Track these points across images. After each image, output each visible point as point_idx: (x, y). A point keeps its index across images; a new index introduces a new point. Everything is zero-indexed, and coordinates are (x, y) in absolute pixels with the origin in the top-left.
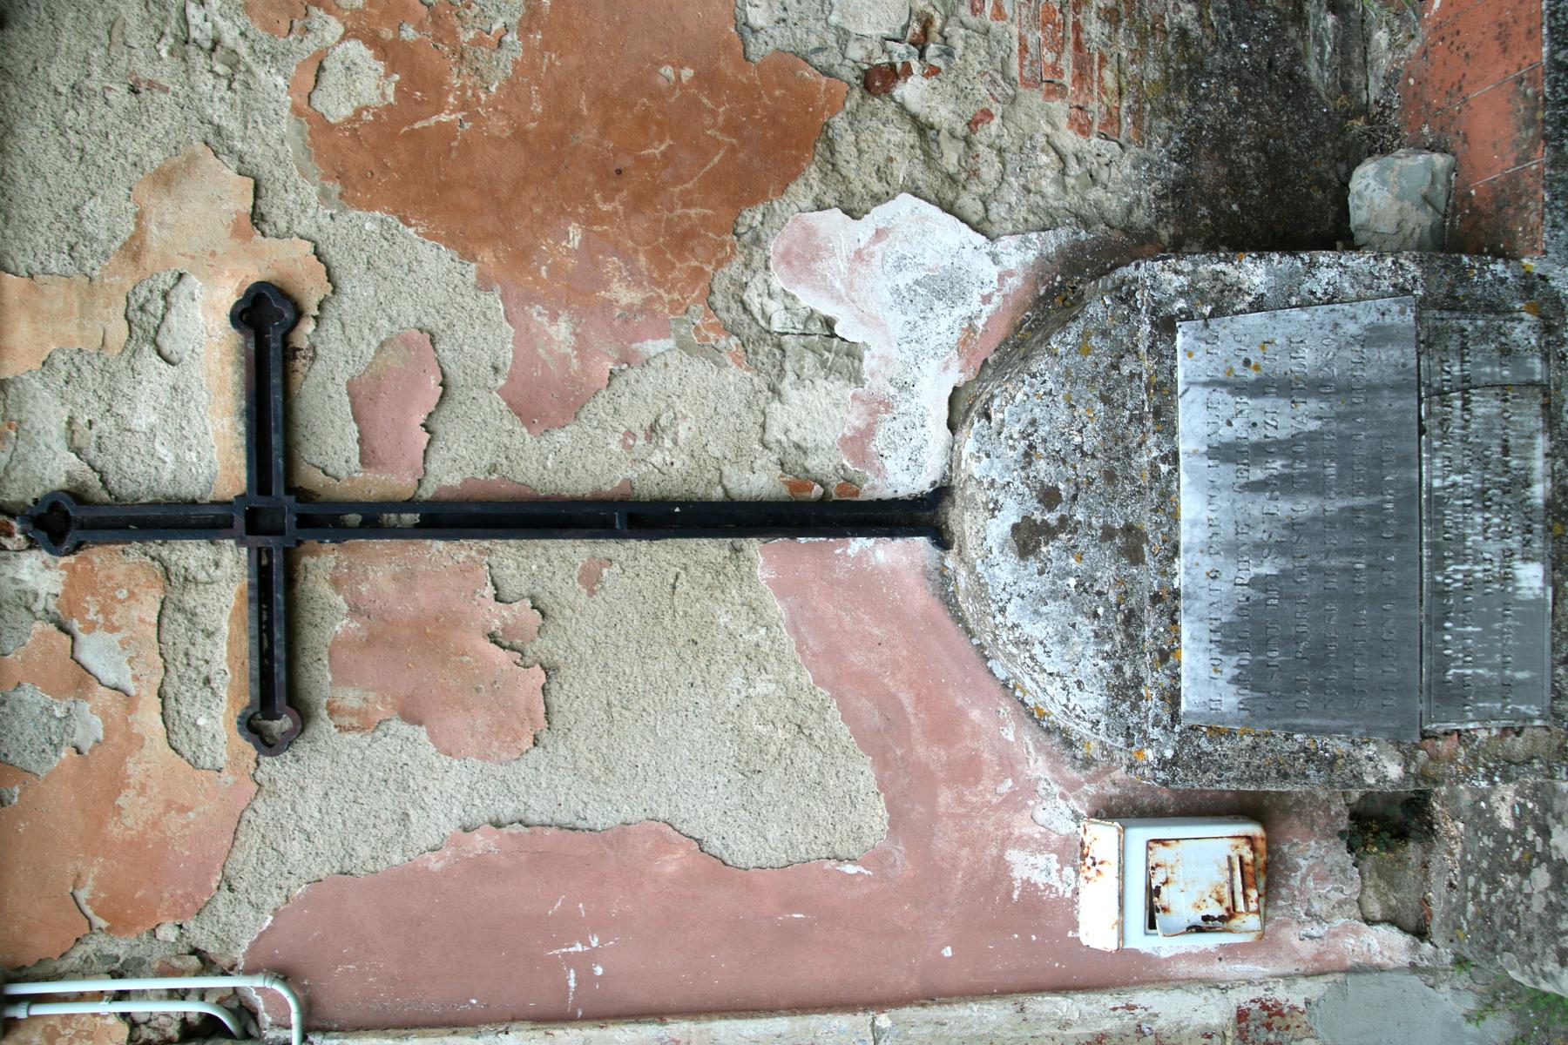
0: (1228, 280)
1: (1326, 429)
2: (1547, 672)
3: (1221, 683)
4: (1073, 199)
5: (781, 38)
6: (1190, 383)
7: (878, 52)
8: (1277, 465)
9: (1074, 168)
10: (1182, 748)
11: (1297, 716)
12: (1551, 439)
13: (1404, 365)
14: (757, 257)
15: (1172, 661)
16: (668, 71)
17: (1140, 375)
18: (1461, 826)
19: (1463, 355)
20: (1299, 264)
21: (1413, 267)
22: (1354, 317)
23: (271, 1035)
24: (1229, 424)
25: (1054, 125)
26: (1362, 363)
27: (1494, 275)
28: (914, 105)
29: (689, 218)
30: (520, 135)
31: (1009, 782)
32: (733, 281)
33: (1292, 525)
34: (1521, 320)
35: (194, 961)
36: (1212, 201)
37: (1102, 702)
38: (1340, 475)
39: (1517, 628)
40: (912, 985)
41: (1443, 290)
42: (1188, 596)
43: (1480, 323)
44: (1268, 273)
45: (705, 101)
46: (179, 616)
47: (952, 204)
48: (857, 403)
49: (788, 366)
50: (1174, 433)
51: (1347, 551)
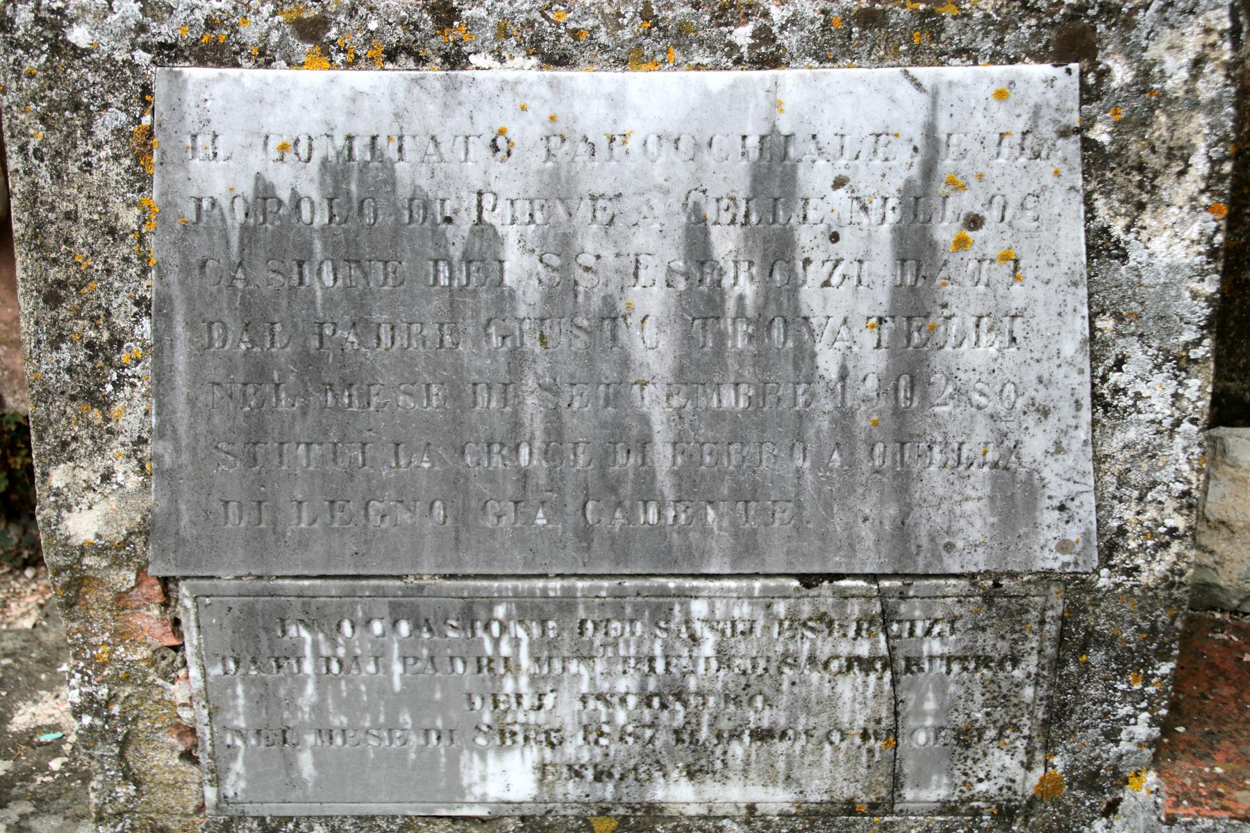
0: (1165, 182)
1: (820, 388)
2: (316, 809)
3: (257, 161)
6: (935, 95)
8: (743, 286)
10: (96, 67)
11: (191, 325)
12: (784, 815)
13: (949, 547)
15: (303, 48)
18: (27, 623)
19: (963, 659)
20: (1189, 335)
21: (1160, 568)
22: (1059, 449)
24: (839, 183)
26: (959, 464)
27: (1126, 720)
33: (611, 316)
34: (1028, 767)
38: (718, 416)
39: (402, 754)
41: (1103, 626)
42: (451, 87)
43: (1028, 692)
44: (1173, 269)
50: (822, 58)
51: (555, 430)
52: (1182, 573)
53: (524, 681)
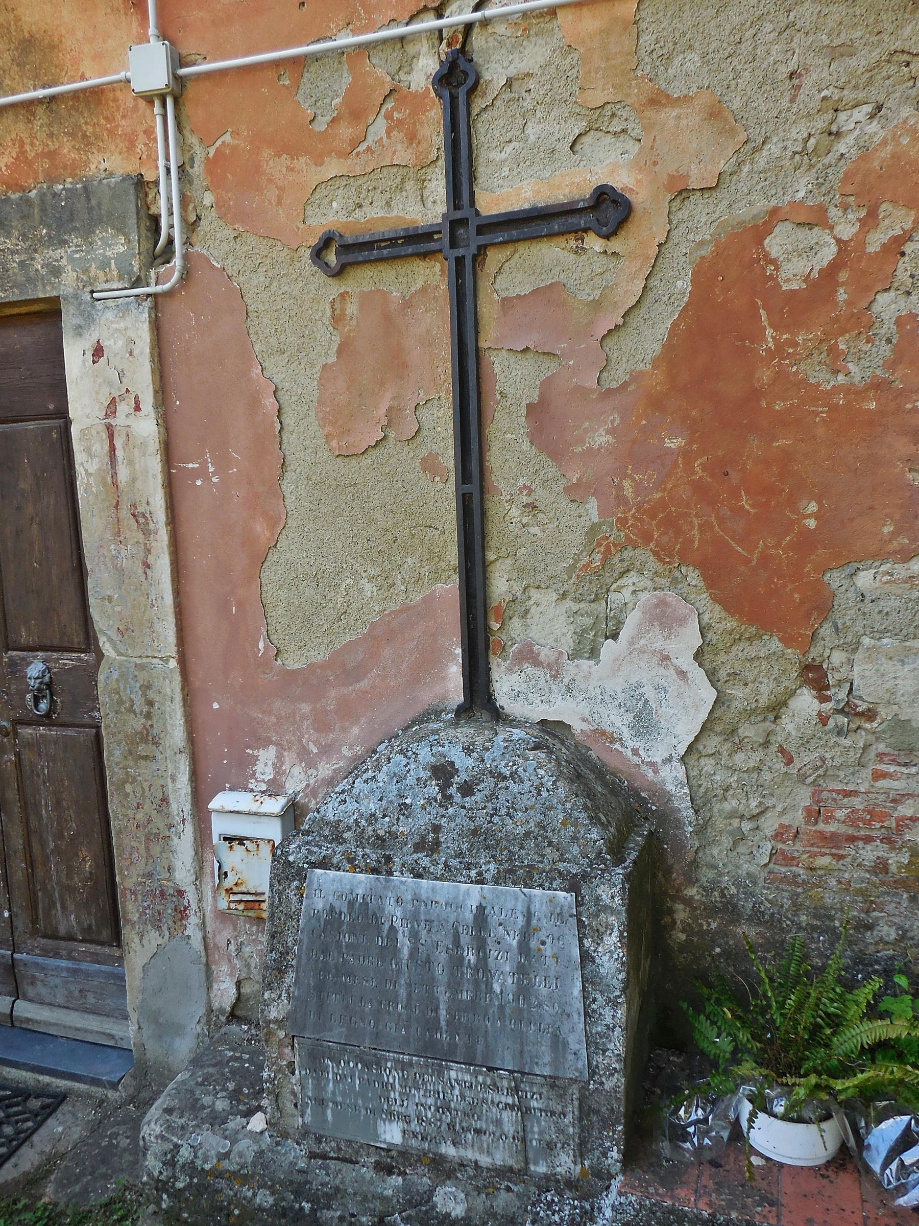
4: (720, 823)
5: (845, 600)
7: (838, 676)
9: (746, 826)
14: (663, 581)
16: (813, 507)
17: (542, 862)
19: (545, 1111)
20: (617, 993)
23: (152, 272)
25: (783, 812)
28: (794, 703)
29: (690, 530)
30: (755, 394)
31: (315, 751)
32: (643, 564)
35: (193, 218)
36: (722, 932)
37: (330, 816)
40: (196, 682)
41: (595, 1106)
43: (571, 1129)
45: (788, 539)
46: (398, 180)
47: (711, 730)
48: (556, 655)
49: (582, 605)
52: (619, 1087)
53: (397, 1093)
